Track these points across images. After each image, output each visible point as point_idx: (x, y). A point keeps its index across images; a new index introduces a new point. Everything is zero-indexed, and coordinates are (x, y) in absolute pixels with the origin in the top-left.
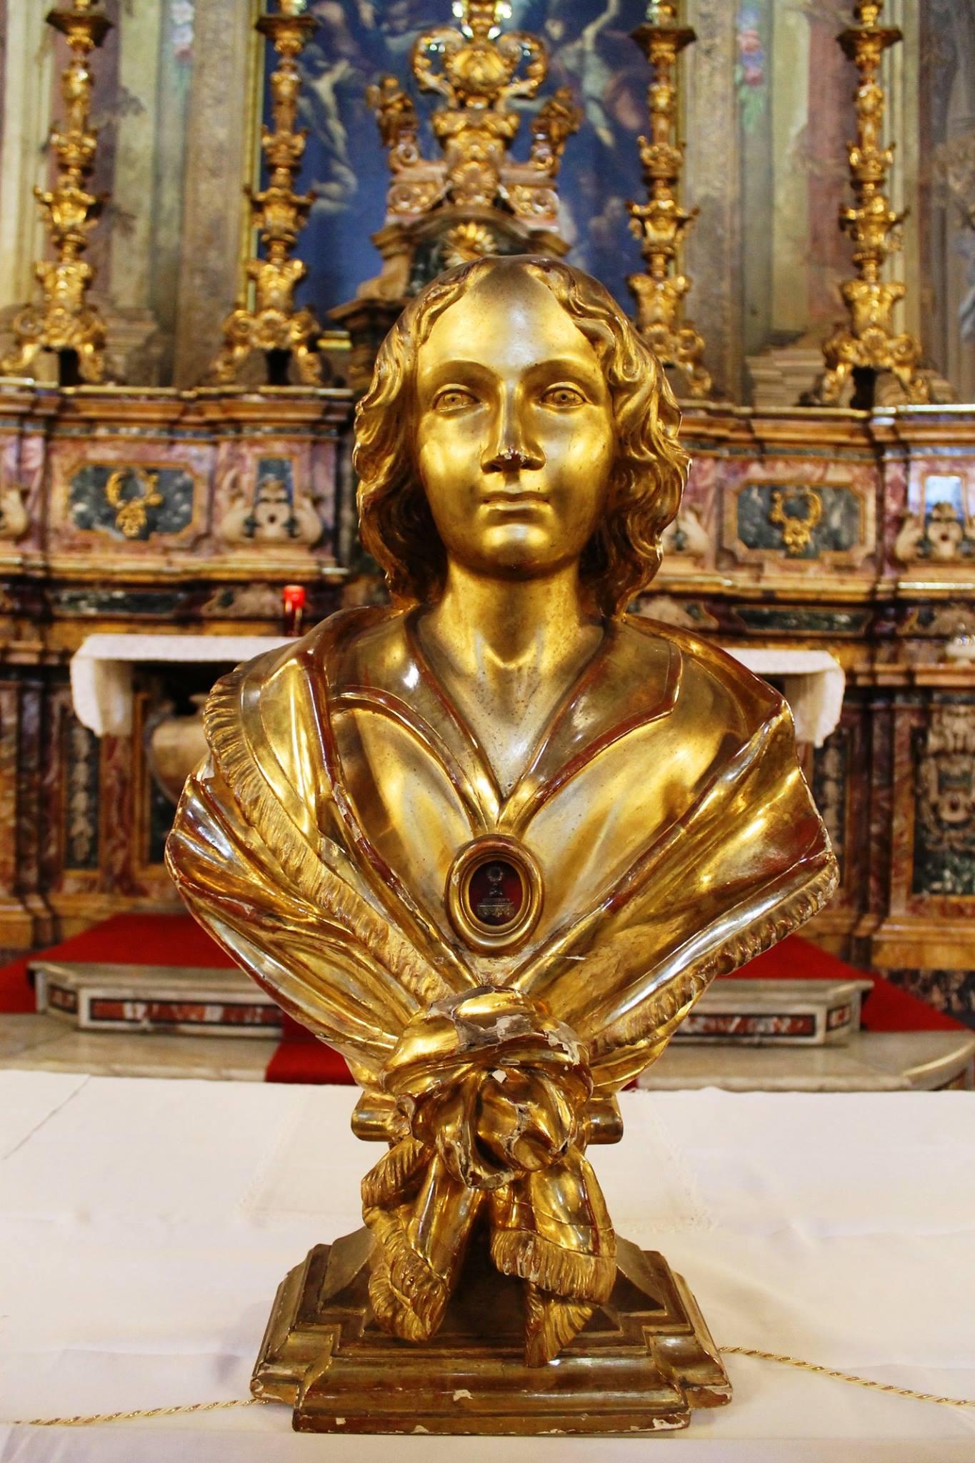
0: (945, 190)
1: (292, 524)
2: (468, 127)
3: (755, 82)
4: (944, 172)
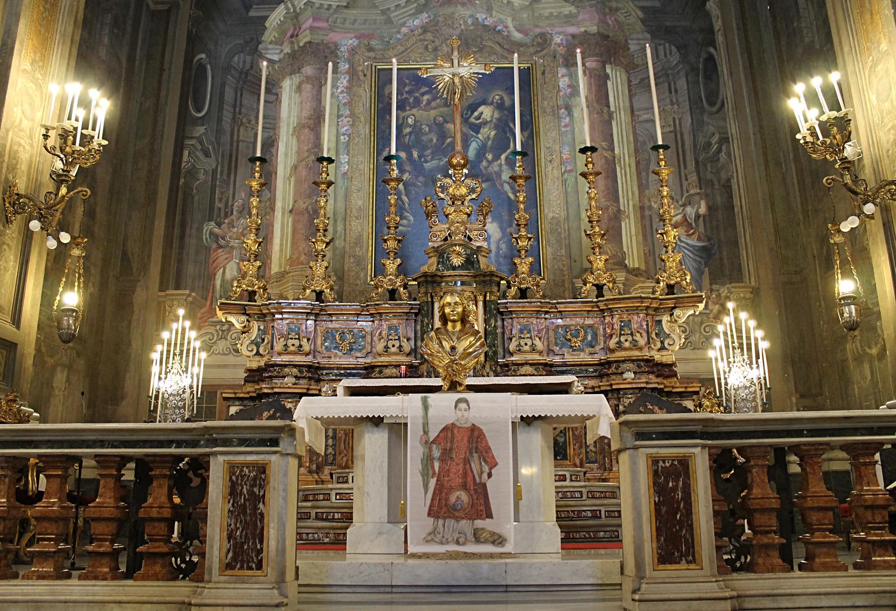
0: (650, 208)
1: (400, 346)
2: (455, 211)
3: (570, 171)
4: (649, 201)
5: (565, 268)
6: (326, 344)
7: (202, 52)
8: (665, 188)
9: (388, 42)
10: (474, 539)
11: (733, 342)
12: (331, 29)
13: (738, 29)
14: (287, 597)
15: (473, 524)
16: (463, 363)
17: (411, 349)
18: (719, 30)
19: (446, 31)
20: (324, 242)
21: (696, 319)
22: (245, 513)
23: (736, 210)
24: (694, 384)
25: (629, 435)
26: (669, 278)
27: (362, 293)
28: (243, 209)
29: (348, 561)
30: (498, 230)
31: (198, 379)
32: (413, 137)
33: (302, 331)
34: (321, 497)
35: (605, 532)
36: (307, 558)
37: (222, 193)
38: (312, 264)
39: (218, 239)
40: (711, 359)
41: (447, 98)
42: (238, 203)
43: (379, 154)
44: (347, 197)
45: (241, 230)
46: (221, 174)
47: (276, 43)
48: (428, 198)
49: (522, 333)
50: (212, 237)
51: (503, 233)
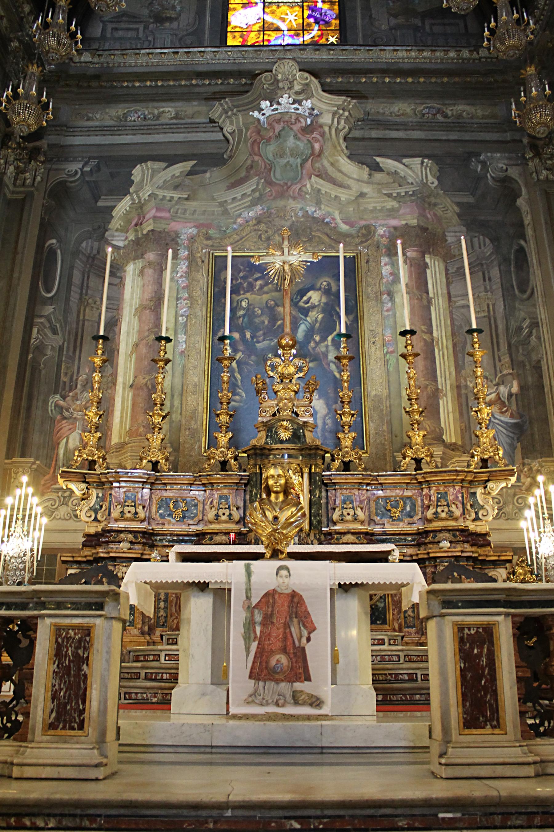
0: (466, 386)
1: (230, 515)
2: (283, 389)
3: (392, 352)
4: (466, 381)
5: (386, 443)
6: (160, 512)
7: (53, 238)
8: (479, 369)
9: (225, 231)
10: (292, 701)
11: (543, 513)
12: (173, 219)
13: (546, 223)
14: (106, 757)
15: (292, 686)
16: (284, 532)
17: (241, 518)
18: (529, 224)
19: (278, 222)
20: (161, 416)
21: (509, 491)
22: (69, 675)
23: (546, 389)
24: (508, 553)
25: (436, 603)
26: (482, 452)
27: (196, 464)
28: (87, 383)
29: (172, 721)
30: (325, 406)
31: (39, 543)
32: (246, 319)
33: (138, 499)
34: (151, 658)
35: (421, 694)
36: (129, 718)
37: (67, 368)
38: (149, 436)
39: (62, 411)
40: (522, 529)
41: (277, 284)
42: (82, 377)
43: (214, 334)
44: (183, 374)
45: (84, 403)
46: (67, 351)
47: (122, 231)
48: (259, 376)
49: (345, 503)
50: (57, 409)
51: (329, 409)
